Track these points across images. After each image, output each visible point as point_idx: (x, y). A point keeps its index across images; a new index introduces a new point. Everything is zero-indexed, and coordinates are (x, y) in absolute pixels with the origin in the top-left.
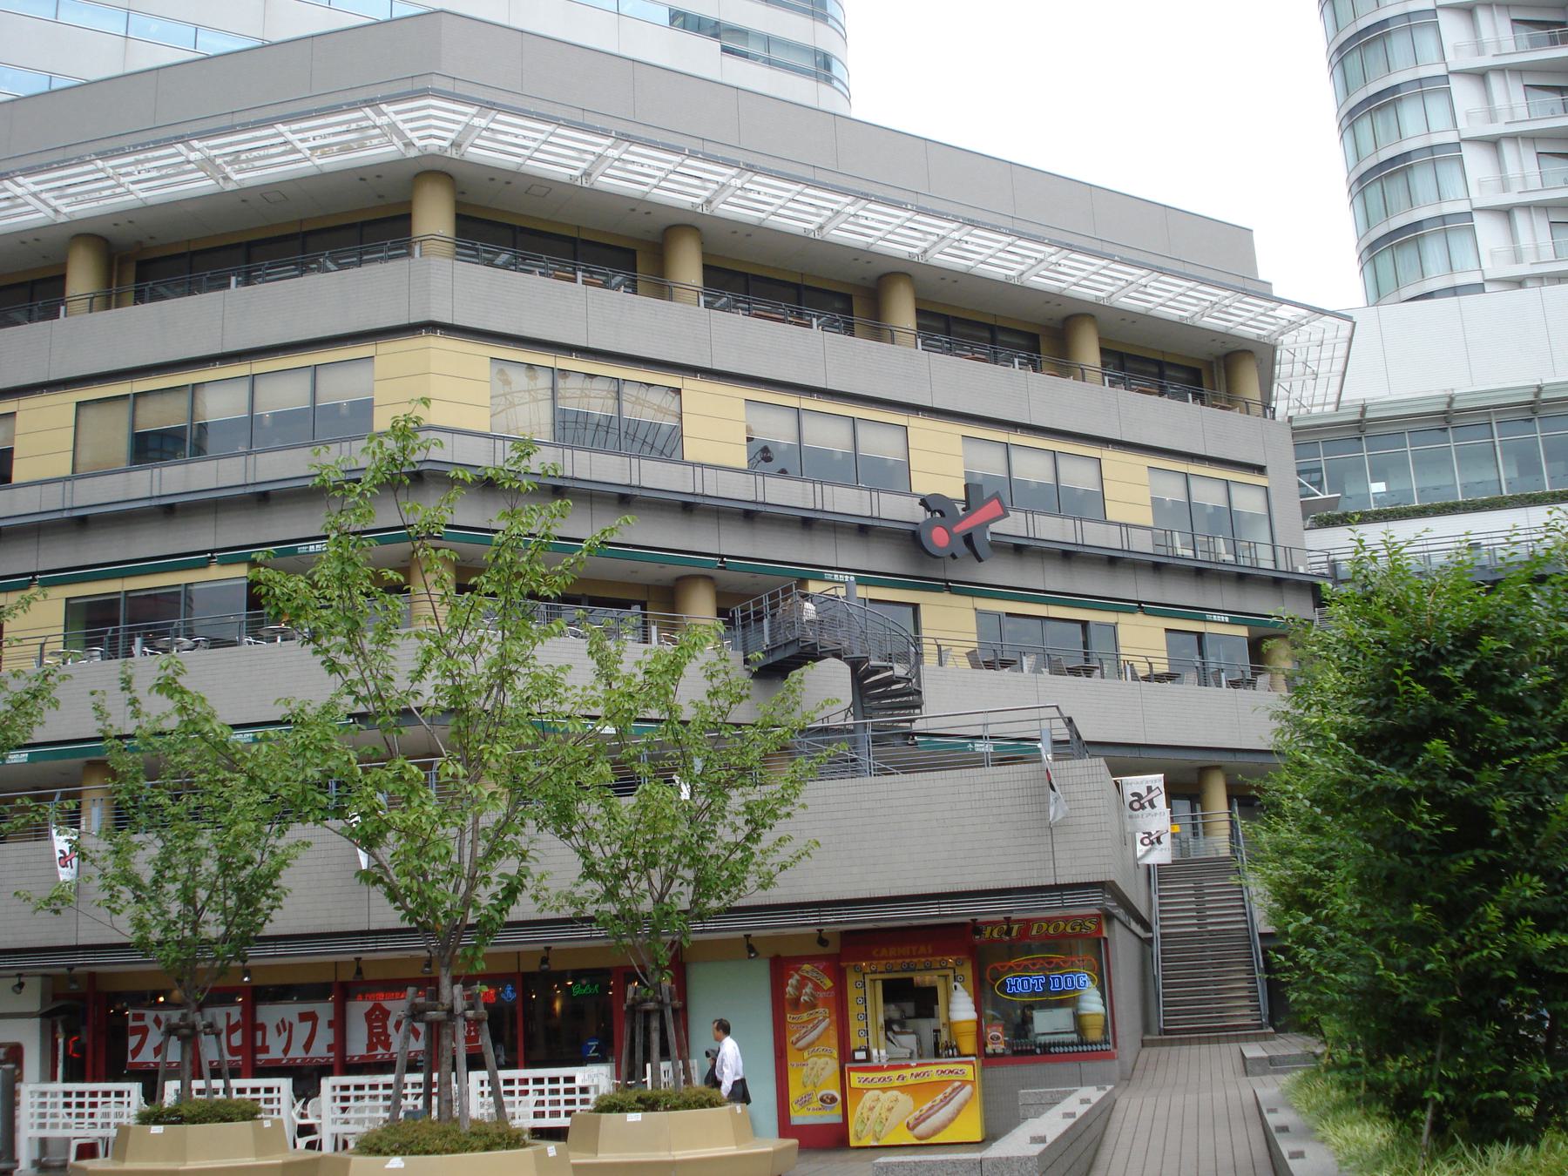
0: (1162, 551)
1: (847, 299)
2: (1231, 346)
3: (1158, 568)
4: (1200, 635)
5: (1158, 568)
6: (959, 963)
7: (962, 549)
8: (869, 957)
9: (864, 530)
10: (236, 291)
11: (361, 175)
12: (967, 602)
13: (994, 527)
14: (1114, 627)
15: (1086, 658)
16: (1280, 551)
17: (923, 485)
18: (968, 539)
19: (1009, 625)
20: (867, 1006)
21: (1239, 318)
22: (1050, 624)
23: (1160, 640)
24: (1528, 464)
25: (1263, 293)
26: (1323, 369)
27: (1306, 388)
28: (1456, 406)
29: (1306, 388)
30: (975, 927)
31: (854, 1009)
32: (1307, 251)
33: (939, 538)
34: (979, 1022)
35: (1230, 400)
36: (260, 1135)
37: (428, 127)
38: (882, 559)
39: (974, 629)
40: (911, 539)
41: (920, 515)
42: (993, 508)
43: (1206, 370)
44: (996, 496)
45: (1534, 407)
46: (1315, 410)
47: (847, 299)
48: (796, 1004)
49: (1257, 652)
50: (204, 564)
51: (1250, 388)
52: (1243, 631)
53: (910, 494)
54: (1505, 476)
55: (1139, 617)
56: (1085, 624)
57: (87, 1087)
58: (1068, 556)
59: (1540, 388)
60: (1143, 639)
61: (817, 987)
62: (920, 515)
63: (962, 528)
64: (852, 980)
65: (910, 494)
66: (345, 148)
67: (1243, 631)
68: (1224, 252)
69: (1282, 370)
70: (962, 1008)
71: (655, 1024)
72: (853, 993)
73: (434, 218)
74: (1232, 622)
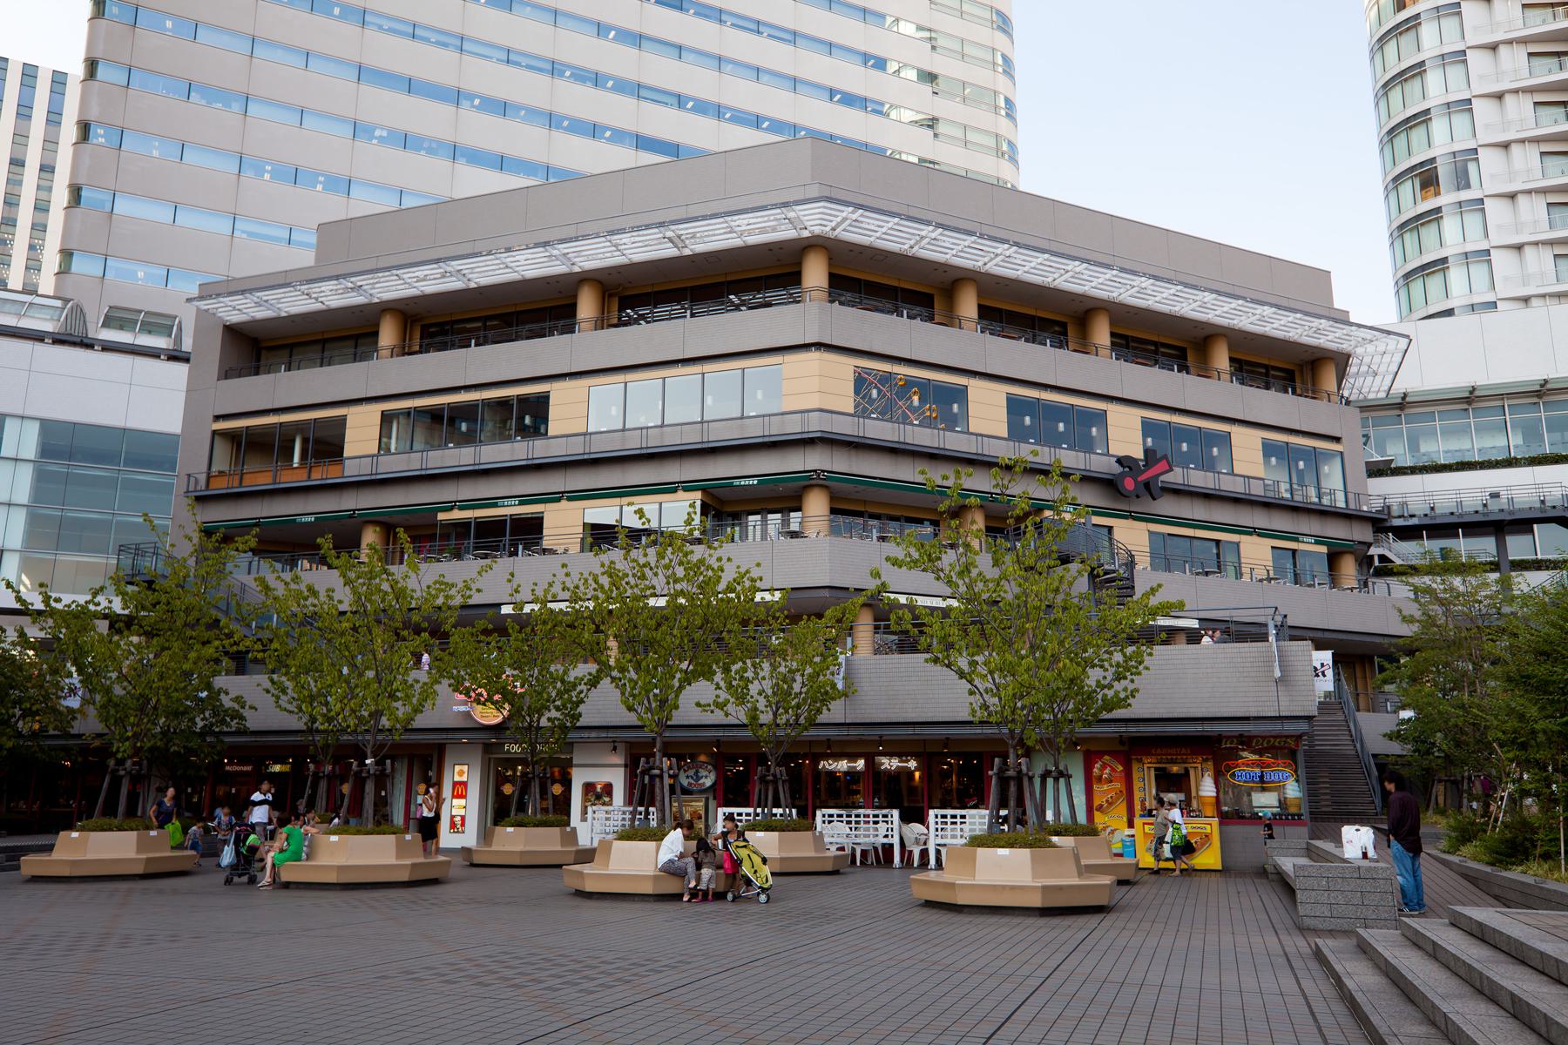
0: (1271, 494)
1: (1064, 325)
2: (1319, 355)
3: (1267, 505)
4: (1294, 551)
5: (1267, 505)
6: (1205, 760)
7: (1143, 490)
8: (1149, 754)
9: (1088, 479)
10: (474, 350)
11: (769, 248)
12: (1143, 525)
13: (1162, 478)
14: (1238, 544)
15: (1219, 561)
16: (1351, 496)
17: (1118, 449)
18: (1147, 485)
19: (1169, 541)
20: (1145, 786)
21: (1326, 337)
22: (1196, 543)
23: (1269, 553)
24: (1531, 432)
25: (1342, 319)
26: (1383, 369)
27: (1366, 383)
28: (1477, 393)
29: (1366, 383)
30: (1219, 738)
31: (1137, 785)
32: (1365, 291)
33: (1129, 484)
34: (1217, 798)
35: (1313, 392)
36: (563, 834)
37: (815, 220)
38: (1089, 496)
39: (1147, 543)
40: (1108, 484)
41: (1118, 469)
42: (1162, 466)
43: (1295, 368)
44: (1165, 457)
45: (1542, 392)
46: (1371, 396)
47: (1064, 325)
48: (1100, 779)
49: (1333, 559)
50: (452, 509)
51: (1329, 381)
52: (1324, 549)
53: (1108, 454)
54: (1516, 443)
55: (1255, 538)
56: (1218, 542)
57: (949, 812)
58: (1208, 497)
59: (1546, 381)
60: (1257, 553)
61: (1113, 770)
62: (1118, 469)
63: (1143, 478)
64: (1135, 767)
65: (1108, 454)
66: (763, 231)
67: (1324, 549)
68: (1307, 289)
69: (1352, 370)
70: (1207, 788)
71: (1013, 788)
72: (1136, 775)
73: (815, 274)
74: (1317, 543)
